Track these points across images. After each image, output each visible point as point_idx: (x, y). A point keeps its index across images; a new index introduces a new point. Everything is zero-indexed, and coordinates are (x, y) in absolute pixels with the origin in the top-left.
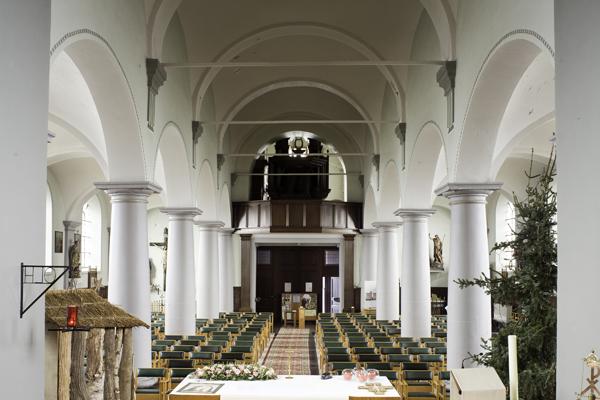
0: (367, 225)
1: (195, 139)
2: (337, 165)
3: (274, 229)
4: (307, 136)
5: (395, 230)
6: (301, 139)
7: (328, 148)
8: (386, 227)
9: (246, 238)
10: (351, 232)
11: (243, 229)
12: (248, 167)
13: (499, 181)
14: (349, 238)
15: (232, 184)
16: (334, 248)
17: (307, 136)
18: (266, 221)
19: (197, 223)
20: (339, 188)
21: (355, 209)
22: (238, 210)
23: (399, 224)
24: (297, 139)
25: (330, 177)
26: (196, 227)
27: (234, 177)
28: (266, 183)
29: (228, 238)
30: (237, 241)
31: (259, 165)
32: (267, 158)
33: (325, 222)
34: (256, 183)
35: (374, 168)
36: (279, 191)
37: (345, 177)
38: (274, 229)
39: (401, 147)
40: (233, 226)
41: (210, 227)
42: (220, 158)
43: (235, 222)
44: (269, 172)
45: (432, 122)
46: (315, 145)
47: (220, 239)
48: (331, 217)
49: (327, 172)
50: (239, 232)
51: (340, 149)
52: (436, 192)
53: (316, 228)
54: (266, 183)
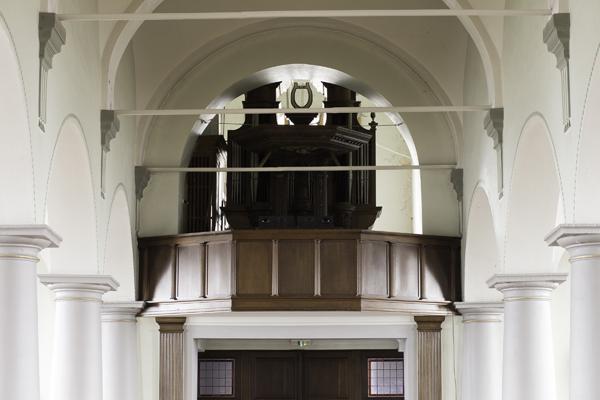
0: (474, 288)
1: (44, 54)
2: (395, 145)
3: (242, 302)
4: (319, 77)
5: (546, 294)
6: (307, 86)
7: (371, 108)
8: (523, 287)
9: (172, 326)
10: (432, 310)
11: (165, 302)
12: (178, 151)
13: (563, 271)
14: (429, 325)
15: (139, 194)
16: (393, 355)
17: (319, 77)
18: (221, 284)
19: (47, 280)
20: (402, 202)
21: (443, 255)
22: (153, 257)
23: (500, 305)
24: (296, 87)
25: (380, 176)
26: (44, 291)
27: (142, 177)
28: (222, 195)
29: (128, 325)
30: (148, 329)
31: (205, 148)
32: (223, 131)
33: (370, 284)
34: (198, 190)
35: (490, 142)
36: (252, 209)
37: (417, 173)
38: (242, 302)
39: (558, 75)
40: (140, 297)
41: (83, 289)
42: (108, 119)
43: (145, 287)
44: (230, 164)
45: (537, 113)
46: (337, 94)
47: (105, 334)
48: (383, 275)
49: (372, 162)
50: (153, 312)
51: (397, 100)
52: (488, 282)
53: (347, 300)
54: (222, 195)
